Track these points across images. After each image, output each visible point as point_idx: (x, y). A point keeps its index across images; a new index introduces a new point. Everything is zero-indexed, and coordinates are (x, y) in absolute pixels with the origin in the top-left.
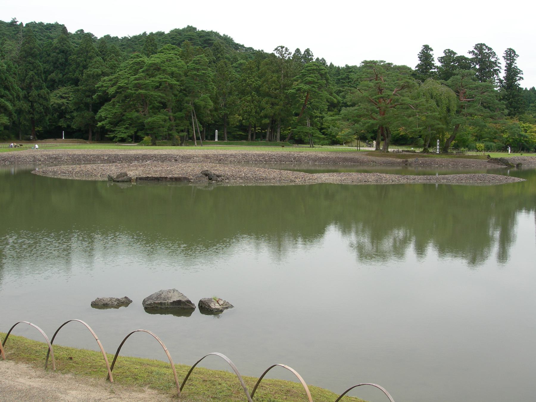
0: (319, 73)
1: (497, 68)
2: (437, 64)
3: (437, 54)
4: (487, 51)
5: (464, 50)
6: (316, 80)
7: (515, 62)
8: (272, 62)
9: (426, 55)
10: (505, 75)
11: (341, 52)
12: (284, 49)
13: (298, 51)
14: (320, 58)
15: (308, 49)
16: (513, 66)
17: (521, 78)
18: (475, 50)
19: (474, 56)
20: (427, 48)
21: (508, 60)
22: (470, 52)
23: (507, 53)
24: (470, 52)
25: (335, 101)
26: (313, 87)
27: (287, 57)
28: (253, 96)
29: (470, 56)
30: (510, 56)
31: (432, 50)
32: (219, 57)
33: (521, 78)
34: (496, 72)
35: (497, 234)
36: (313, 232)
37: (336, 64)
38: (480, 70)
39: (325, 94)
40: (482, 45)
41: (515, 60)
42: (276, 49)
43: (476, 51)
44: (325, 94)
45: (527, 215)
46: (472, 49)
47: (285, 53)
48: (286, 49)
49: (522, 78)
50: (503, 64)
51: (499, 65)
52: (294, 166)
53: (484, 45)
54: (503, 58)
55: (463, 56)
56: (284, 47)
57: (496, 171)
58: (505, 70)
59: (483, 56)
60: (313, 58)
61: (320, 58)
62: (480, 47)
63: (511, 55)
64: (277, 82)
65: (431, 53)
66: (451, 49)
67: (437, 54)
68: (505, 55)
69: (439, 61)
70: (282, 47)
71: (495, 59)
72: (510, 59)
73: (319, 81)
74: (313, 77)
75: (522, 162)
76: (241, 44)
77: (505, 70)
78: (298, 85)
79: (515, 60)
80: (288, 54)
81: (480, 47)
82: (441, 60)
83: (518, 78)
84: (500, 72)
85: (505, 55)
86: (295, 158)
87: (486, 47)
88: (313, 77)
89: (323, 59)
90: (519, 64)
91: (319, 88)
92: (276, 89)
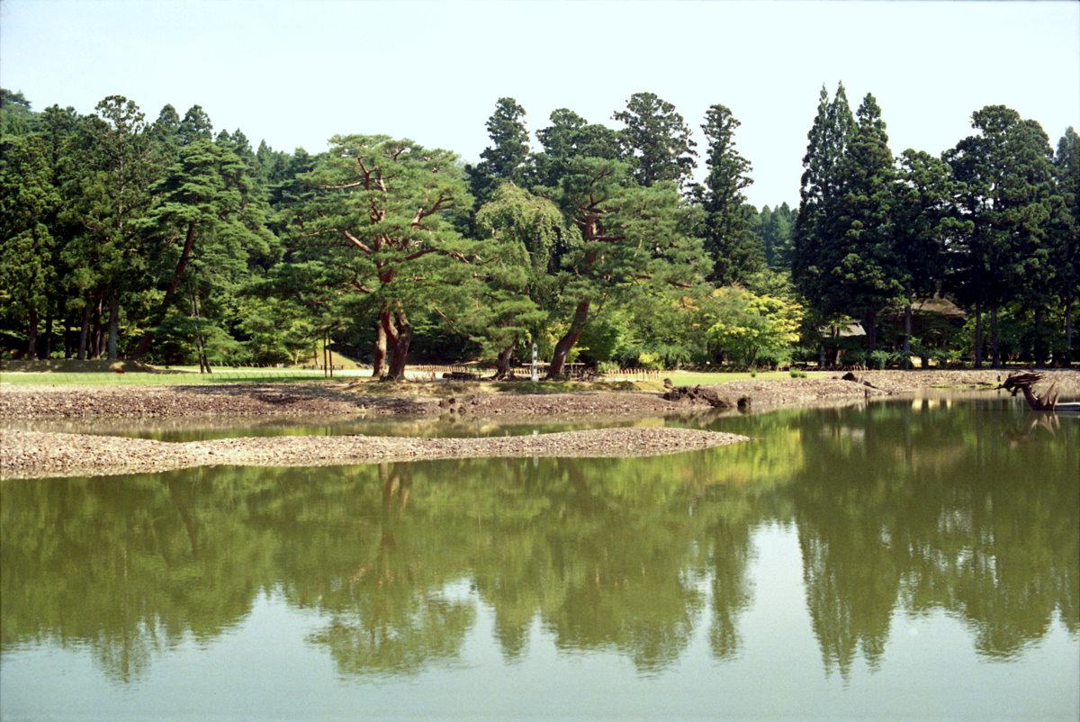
0: (221, 172)
1: (685, 155)
2: (536, 147)
3: (535, 121)
4: (660, 112)
5: (602, 110)
6: (214, 193)
7: (732, 139)
8: (90, 139)
9: (505, 120)
10: (708, 173)
11: (283, 110)
12: (124, 106)
13: (168, 111)
14: (231, 132)
15: (196, 107)
16: (727, 152)
17: (748, 181)
18: (629, 111)
19: (627, 126)
20: (508, 107)
21: (713, 134)
22: (619, 116)
23: (711, 119)
24: (619, 116)
25: (266, 249)
26: (205, 210)
27: (136, 129)
28: (36, 237)
29: (619, 126)
30: (719, 126)
31: (523, 112)
32: (277, 199)
33: (748, 181)
34: (686, 165)
35: (706, 586)
36: (215, 610)
37: (276, 148)
38: (644, 162)
39: (236, 226)
40: (648, 97)
41: (730, 134)
42: (104, 104)
43: (633, 114)
44: (236, 226)
45: (783, 530)
46: (623, 108)
47: (128, 117)
48: (131, 106)
49: (752, 182)
50: (702, 145)
51: (692, 148)
52: (148, 424)
53: (653, 96)
54: (702, 130)
55: (601, 127)
56: (124, 100)
57: (690, 421)
58: (708, 162)
59: (649, 125)
60: (212, 132)
61: (231, 132)
62: (643, 103)
63: (720, 122)
64: (105, 197)
65: (520, 120)
66: (571, 108)
67: (535, 121)
68: (706, 123)
69: (541, 141)
70: (120, 100)
71: (683, 133)
72: (720, 134)
73: (224, 194)
74: (204, 184)
75: (754, 394)
76: (14, 92)
77: (708, 162)
78: (163, 205)
79: (730, 134)
80: (137, 119)
81: (643, 103)
82: (546, 136)
83: (740, 181)
84: (695, 166)
85: (706, 123)
86: (148, 402)
87: (659, 102)
88: (204, 184)
89: (238, 133)
90: (742, 143)
91: (223, 214)
92: (103, 216)
